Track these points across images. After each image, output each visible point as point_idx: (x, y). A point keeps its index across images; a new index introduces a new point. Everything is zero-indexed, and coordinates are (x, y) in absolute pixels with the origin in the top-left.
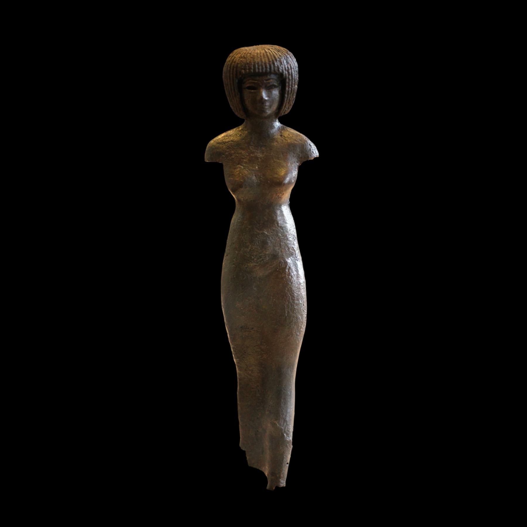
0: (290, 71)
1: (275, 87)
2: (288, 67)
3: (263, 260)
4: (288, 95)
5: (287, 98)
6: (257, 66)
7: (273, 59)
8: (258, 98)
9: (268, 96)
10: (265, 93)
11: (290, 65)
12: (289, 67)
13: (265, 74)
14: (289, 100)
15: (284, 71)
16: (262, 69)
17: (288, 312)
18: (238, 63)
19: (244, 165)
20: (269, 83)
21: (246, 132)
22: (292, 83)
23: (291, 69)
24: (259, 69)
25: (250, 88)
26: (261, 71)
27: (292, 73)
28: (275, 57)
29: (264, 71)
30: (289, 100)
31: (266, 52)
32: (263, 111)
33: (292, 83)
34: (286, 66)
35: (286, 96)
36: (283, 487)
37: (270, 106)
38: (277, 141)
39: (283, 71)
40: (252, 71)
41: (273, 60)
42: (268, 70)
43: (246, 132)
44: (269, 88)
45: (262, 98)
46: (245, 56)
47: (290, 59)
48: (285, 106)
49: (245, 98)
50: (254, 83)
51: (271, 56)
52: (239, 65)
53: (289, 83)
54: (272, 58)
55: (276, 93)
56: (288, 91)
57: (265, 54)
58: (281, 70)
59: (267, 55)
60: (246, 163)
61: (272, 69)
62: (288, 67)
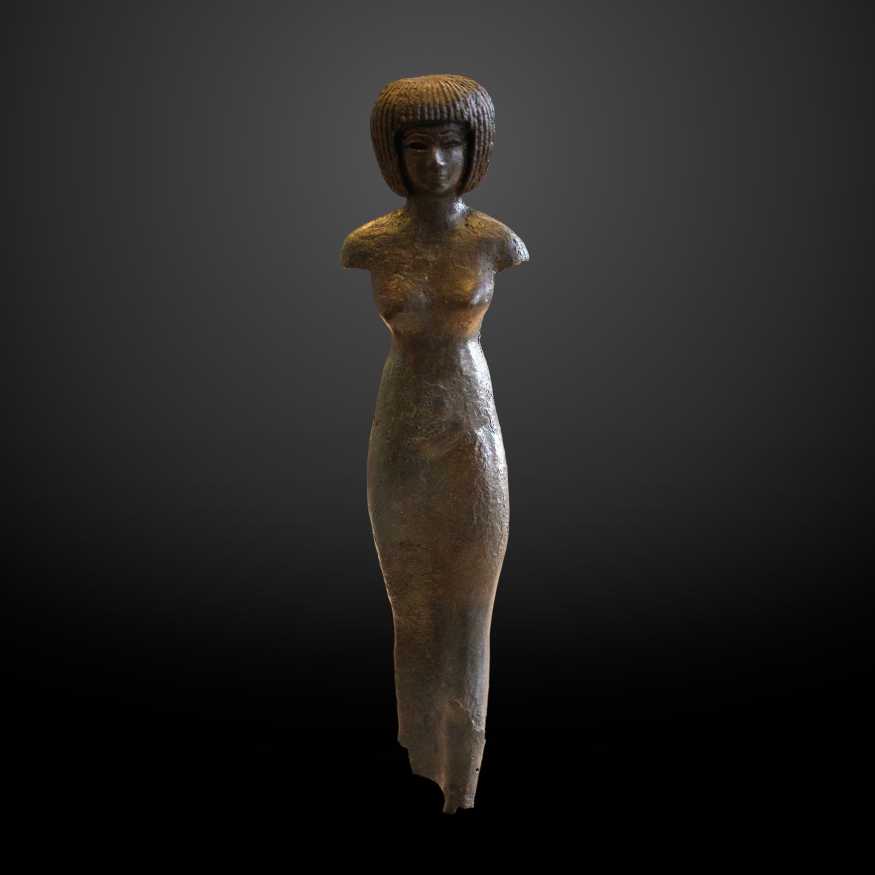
0: (482, 118)
1: (457, 144)
2: (478, 112)
3: (436, 431)
4: (478, 157)
5: (477, 162)
6: (426, 110)
7: (454, 97)
8: (429, 163)
9: (445, 160)
10: (440, 154)
11: (482, 108)
12: (480, 111)
13: (441, 123)
14: (481, 166)
15: (472, 118)
16: (436, 114)
17: (479, 518)
18: (395, 105)
19: (406, 273)
20: (446, 138)
21: (409, 219)
22: (485, 137)
23: (483, 114)
24: (429, 114)
25: (415, 146)
26: (433, 117)
27: (484, 121)
28: (456, 95)
29: (438, 117)
31: (442, 87)
32: (436, 184)
33: (485, 137)
34: (475, 110)
35: (475, 159)
36: (470, 809)
37: (449, 177)
38: (459, 235)
39: (469, 117)
40: (419, 117)
41: (453, 100)
42: (446, 116)
43: (409, 219)
44: (447, 147)
45: (435, 162)
46: (407, 94)
47: (482, 97)
48: (473, 177)
49: (407, 163)
50: (422, 138)
51: (450, 93)
52: (397, 109)
53: (479, 138)
54: (451, 96)
55: (458, 154)
56: (479, 151)
57: (440, 90)
58: (466, 117)
59: (443, 91)
60: (408, 270)
61: (452, 114)
62: (478, 112)
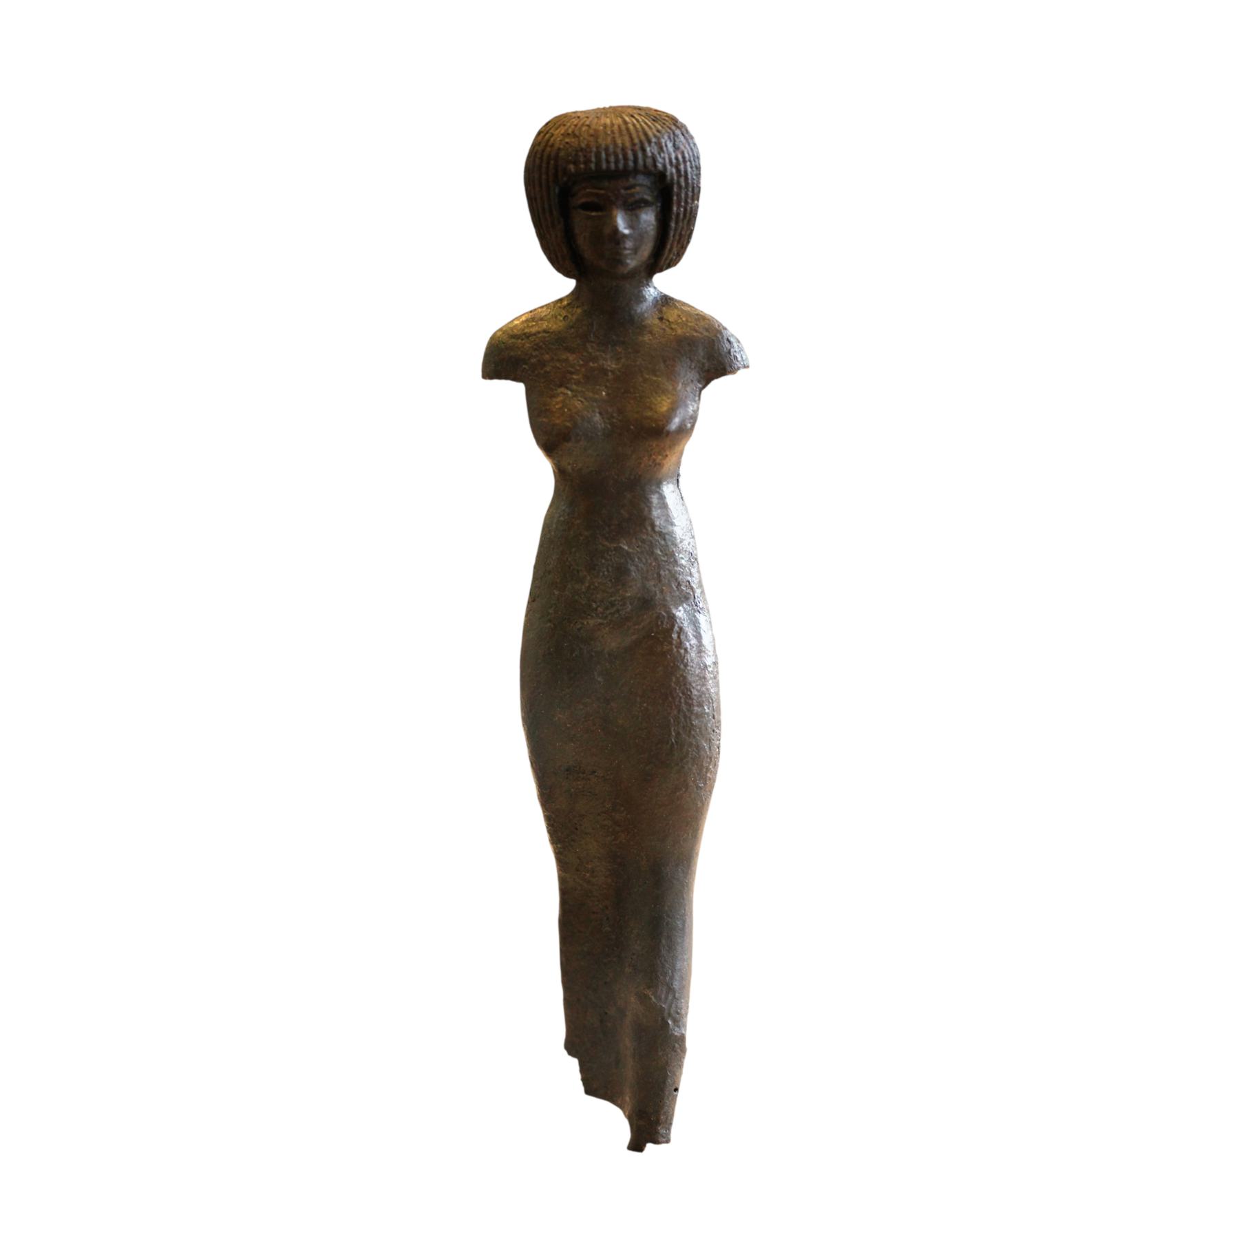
0: (682, 167)
1: (647, 204)
2: (677, 158)
3: (618, 611)
4: (677, 223)
5: (676, 229)
6: (603, 155)
7: (643, 138)
8: (607, 231)
9: (631, 227)
10: (624, 219)
11: (683, 153)
12: (680, 157)
13: (624, 174)
14: (681, 235)
15: (668, 167)
16: (617, 162)
17: (678, 734)
18: (559, 149)
19: (574, 387)
20: (632, 195)
21: (579, 311)
22: (686, 194)
23: (685, 162)
24: (608, 162)
25: (587, 207)
26: (613, 166)
27: (686, 172)
28: (646, 134)
29: (621, 166)
30: (681, 235)
31: (625, 123)
32: (617, 260)
33: (686, 194)
34: (673, 156)
35: (673, 225)
37: (636, 250)
38: (651, 332)
39: (664, 166)
40: (593, 166)
41: (641, 142)
42: (631, 164)
43: (579, 311)
44: (632, 208)
45: (616, 230)
46: (577, 133)
48: (670, 250)
49: (577, 231)
50: (597, 195)
51: (637, 131)
52: (562, 154)
53: (679, 195)
54: (638, 137)
55: (648, 218)
56: (678, 214)
57: (623, 127)
58: (660, 166)
59: (628, 129)
60: (578, 383)
61: (640, 161)
62: (677, 158)
